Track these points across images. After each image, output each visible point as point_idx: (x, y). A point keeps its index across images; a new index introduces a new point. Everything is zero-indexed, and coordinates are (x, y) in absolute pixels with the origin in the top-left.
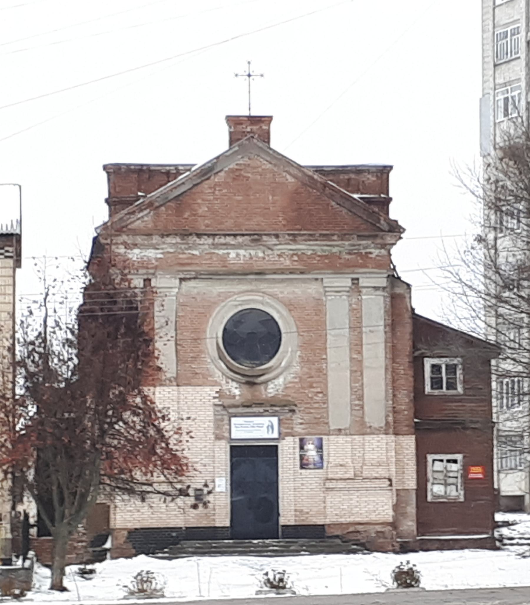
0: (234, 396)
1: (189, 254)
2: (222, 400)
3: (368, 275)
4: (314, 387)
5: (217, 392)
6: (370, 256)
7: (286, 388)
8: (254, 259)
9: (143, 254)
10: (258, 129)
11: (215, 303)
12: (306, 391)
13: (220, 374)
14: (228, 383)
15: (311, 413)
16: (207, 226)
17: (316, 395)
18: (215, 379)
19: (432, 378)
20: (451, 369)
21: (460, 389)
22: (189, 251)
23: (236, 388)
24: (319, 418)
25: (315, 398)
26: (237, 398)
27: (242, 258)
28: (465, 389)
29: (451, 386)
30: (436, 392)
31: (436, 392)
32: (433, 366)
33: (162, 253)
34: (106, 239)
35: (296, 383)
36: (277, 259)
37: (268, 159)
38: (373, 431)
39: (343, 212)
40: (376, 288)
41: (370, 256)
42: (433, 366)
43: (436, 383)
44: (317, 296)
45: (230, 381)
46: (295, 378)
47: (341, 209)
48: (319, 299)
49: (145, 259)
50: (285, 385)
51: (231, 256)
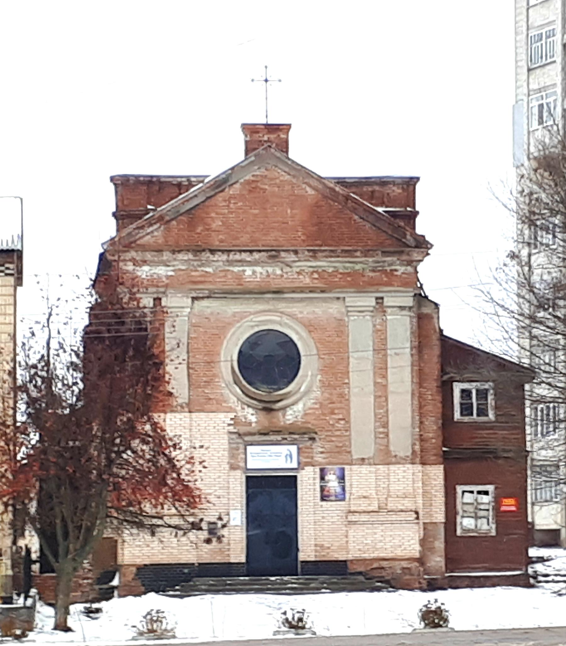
0: (250, 424)
1: (202, 271)
2: (237, 428)
3: (393, 294)
4: (335, 414)
5: (232, 419)
6: (396, 273)
7: (306, 414)
8: (272, 276)
9: (152, 272)
10: (276, 138)
11: (230, 324)
12: (327, 418)
13: (235, 399)
14: (243, 409)
15: (333, 441)
16: (221, 241)
17: (337, 422)
18: (230, 405)
19: (461, 404)
20: (483, 394)
21: (491, 416)
22: (202, 268)
23: (252, 414)
24: (341, 447)
25: (337, 425)
26: (253, 425)
27: (258, 275)
28: (497, 416)
29: (482, 412)
30: (466, 419)
31: (466, 419)
32: (463, 391)
33: (173, 271)
34: (113, 255)
35: (316, 409)
36: (296, 276)
37: (287, 170)
38: (399, 461)
39: (367, 227)
40: (402, 308)
41: (396, 273)
42: (463, 391)
43: (466, 409)
44: (338, 316)
45: (246, 407)
46: (316, 403)
47: (365, 223)
48: (341, 320)
49: (155, 276)
50: (305, 411)
51: (247, 274)
